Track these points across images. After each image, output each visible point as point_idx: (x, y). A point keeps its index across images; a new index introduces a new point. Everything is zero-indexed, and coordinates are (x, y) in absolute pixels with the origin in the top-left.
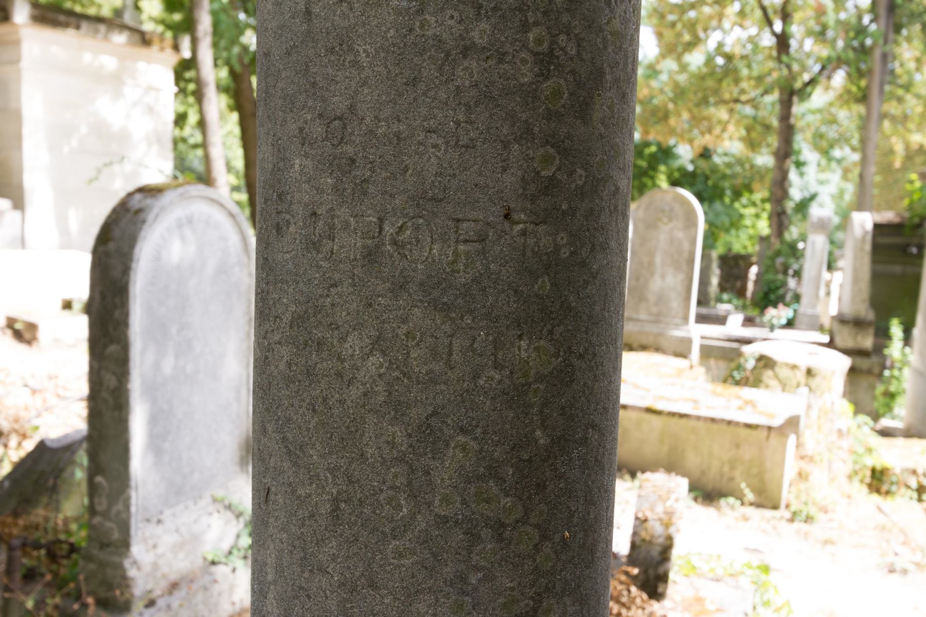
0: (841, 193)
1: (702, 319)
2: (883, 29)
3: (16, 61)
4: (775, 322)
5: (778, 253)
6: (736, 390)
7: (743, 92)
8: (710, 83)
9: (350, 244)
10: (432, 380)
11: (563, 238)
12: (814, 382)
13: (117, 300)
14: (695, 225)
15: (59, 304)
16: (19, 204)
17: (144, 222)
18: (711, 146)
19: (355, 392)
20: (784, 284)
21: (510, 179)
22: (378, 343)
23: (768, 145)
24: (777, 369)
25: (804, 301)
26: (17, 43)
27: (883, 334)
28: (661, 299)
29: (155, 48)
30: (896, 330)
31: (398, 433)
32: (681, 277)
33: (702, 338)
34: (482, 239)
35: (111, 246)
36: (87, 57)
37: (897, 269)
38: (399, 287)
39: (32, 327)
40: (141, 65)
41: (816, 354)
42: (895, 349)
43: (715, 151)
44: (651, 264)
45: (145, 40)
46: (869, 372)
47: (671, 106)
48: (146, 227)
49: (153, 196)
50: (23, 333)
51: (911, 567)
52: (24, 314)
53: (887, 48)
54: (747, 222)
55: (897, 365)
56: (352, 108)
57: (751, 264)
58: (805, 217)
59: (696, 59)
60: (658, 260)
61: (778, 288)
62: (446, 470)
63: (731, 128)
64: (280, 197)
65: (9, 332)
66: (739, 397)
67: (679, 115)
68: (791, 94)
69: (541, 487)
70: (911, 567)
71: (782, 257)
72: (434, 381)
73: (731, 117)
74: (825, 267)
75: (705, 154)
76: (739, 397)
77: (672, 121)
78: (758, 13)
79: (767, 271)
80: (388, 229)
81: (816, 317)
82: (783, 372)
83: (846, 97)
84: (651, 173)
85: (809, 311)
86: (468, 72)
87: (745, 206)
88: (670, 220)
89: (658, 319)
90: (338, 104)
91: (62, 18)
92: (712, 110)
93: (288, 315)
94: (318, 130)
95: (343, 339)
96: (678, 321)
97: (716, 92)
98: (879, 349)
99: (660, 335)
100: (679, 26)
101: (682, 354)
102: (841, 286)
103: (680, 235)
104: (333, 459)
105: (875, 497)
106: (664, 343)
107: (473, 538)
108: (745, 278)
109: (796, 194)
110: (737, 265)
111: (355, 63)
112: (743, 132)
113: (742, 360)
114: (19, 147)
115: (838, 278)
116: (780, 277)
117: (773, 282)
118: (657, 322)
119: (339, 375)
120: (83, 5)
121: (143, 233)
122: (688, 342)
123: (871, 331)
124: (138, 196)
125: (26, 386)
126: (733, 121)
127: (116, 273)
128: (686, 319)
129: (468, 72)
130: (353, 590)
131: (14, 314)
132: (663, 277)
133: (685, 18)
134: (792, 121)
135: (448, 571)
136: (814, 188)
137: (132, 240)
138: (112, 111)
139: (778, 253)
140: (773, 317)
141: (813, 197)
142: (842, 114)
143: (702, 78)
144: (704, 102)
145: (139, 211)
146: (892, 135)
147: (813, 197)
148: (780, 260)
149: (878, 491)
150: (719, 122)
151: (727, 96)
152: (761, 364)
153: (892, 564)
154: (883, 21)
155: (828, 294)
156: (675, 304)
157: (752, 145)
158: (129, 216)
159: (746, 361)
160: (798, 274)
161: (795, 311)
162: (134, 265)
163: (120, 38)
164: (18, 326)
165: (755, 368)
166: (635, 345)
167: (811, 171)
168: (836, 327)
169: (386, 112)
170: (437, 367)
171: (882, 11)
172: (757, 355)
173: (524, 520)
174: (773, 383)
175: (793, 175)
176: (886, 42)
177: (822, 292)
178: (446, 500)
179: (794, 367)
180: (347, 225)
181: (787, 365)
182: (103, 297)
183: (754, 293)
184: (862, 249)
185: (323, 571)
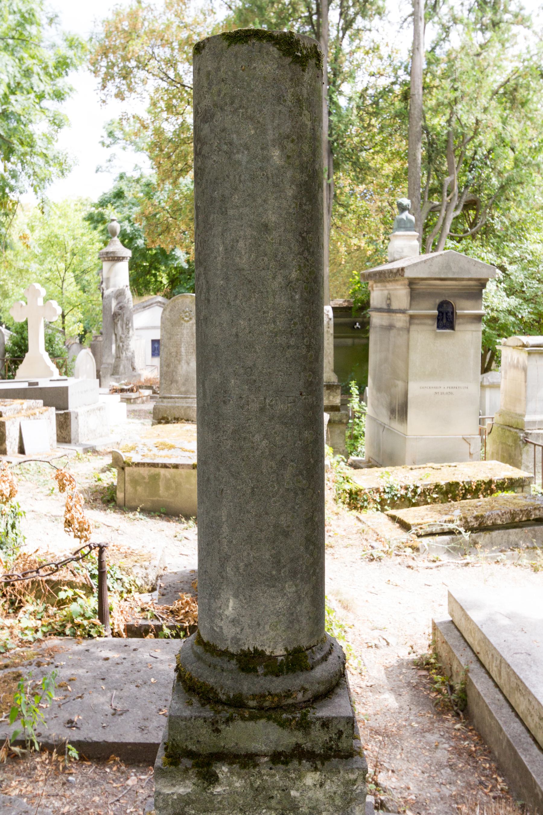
9: (255, 406)
10: (283, 446)
11: (314, 399)
19: (258, 453)
21: (301, 383)
22: (266, 436)
27: (346, 392)
30: (355, 390)
31: (273, 464)
34: (294, 402)
37: (349, 341)
38: (271, 418)
42: (355, 403)
46: (340, 422)
51: (382, 554)
55: (357, 415)
56: (254, 365)
60: (183, 350)
62: (288, 474)
64: (225, 392)
69: (313, 476)
70: (382, 554)
72: (283, 447)
80: (267, 401)
86: (289, 353)
90: (249, 363)
93: (231, 430)
94: (242, 371)
95: (253, 436)
98: (345, 403)
104: (251, 475)
105: (354, 512)
107: (296, 494)
111: (255, 352)
119: (253, 448)
123: (339, 391)
129: (289, 353)
130: (260, 516)
135: (289, 506)
149: (356, 508)
153: (372, 555)
169: (266, 366)
170: (284, 442)
173: (308, 488)
178: (288, 483)
180: (253, 401)
185: (248, 512)
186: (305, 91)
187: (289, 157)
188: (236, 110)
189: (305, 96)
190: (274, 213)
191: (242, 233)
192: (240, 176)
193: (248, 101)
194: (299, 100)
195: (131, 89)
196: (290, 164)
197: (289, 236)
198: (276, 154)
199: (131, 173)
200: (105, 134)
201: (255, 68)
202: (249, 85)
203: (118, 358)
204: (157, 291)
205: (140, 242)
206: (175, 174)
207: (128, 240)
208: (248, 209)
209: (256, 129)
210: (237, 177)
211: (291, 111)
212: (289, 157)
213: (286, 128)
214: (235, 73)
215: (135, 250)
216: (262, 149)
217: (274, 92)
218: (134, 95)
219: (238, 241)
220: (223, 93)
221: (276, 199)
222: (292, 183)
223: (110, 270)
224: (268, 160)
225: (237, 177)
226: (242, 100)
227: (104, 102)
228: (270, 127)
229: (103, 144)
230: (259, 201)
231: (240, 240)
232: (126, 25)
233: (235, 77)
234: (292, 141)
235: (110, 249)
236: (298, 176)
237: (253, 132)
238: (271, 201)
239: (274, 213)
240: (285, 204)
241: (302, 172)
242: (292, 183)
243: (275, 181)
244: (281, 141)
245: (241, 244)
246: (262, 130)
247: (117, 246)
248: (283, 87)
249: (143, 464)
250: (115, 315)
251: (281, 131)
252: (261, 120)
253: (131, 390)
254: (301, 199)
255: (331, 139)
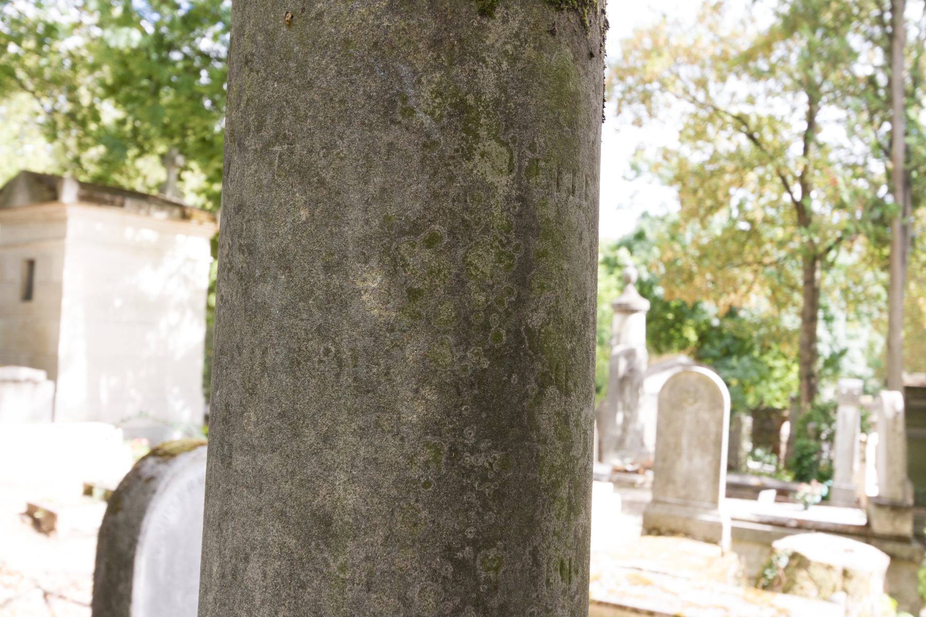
0: (871, 346)
1: (735, 490)
2: (901, 203)
3: (62, 237)
4: (808, 499)
5: (809, 419)
6: (767, 596)
7: (766, 254)
8: (732, 247)
12: (851, 585)
13: (122, 573)
14: (720, 406)
15: (81, 490)
16: (52, 375)
17: (154, 492)
18: (736, 304)
20: (820, 451)
23: (794, 305)
24: (811, 569)
25: (839, 474)
26: (63, 220)
28: (689, 481)
29: (194, 222)
32: (708, 459)
33: (733, 519)
35: (121, 516)
36: (129, 233)
39: (51, 516)
40: (180, 238)
41: (851, 551)
43: (741, 309)
44: (677, 445)
45: (185, 216)
47: (695, 269)
48: (156, 497)
49: (166, 462)
50: (41, 522)
52: (45, 504)
53: (906, 221)
54: (777, 374)
57: (783, 420)
58: (837, 369)
59: (719, 221)
60: (684, 441)
61: (810, 455)
63: (756, 287)
65: (28, 520)
66: (772, 606)
67: (703, 275)
68: (814, 259)
71: (816, 421)
73: (756, 277)
74: (858, 429)
75: (731, 313)
76: (772, 606)
77: (698, 281)
78: (778, 180)
79: (798, 436)
81: (850, 492)
82: (818, 573)
83: (869, 259)
84: (678, 325)
85: (844, 486)
87: (775, 358)
88: (696, 401)
89: (686, 502)
91: (107, 197)
92: (736, 271)
96: (707, 504)
97: (740, 253)
99: (688, 519)
100: (701, 193)
101: (712, 539)
102: (877, 448)
103: (706, 416)
106: (693, 528)
108: (777, 431)
109: (824, 349)
110: (769, 419)
112: (769, 292)
113: (774, 558)
114: (58, 319)
115: (874, 439)
116: (812, 443)
117: (806, 447)
118: (685, 505)
120: (129, 178)
121: (152, 504)
122: (718, 527)
124: (151, 461)
125: (38, 587)
126: (758, 281)
127: (123, 546)
128: (715, 502)
131: (35, 501)
132: (690, 458)
133: (706, 185)
134: (816, 284)
136: (843, 343)
137: (141, 512)
138: (150, 281)
139: (809, 419)
140: (806, 494)
141: (843, 353)
142: (868, 276)
143: (723, 241)
144: (728, 261)
145: (151, 479)
146: (920, 296)
147: (843, 353)
148: (811, 426)
150: (744, 282)
151: (750, 258)
152: (795, 562)
154: (900, 195)
155: (864, 460)
156: (704, 487)
157: (779, 304)
158: (140, 484)
159: (778, 558)
160: (831, 438)
161: (829, 488)
162: (141, 538)
163: (160, 215)
164: (38, 515)
165: (787, 567)
166: (663, 529)
167: (840, 326)
168: (873, 510)
171: (899, 186)
172: (789, 553)
174: (808, 585)
175: (821, 330)
176: (904, 215)
177: (857, 465)
179: (829, 567)
181: (821, 564)
182: (109, 569)
183: (787, 455)
184: (894, 430)
186: (488, 80)
187: (414, 294)
188: (267, 147)
189: (490, 92)
190: (352, 480)
191: (258, 535)
192: (265, 352)
193: (299, 119)
194: (461, 108)
195: (651, 115)
196: (416, 316)
197: (405, 559)
198: (370, 284)
199: (655, 212)
200: (628, 168)
201: (320, 15)
202: (302, 67)
203: (624, 429)
204: (683, 348)
205: (659, 291)
206: (702, 211)
207: (645, 289)
208: (277, 459)
209: (313, 203)
210: (258, 352)
211: (429, 145)
212: (414, 294)
213: (410, 201)
214: (270, 36)
215: (655, 301)
216: (327, 268)
217: (373, 86)
218: (654, 121)
219: (247, 559)
220: (245, 98)
221: (362, 433)
222: (423, 381)
223: (622, 324)
224: (344, 305)
225: (258, 352)
226: (281, 116)
227: (618, 130)
228: (355, 197)
229: (624, 178)
230: (310, 436)
231: (253, 558)
232: (647, 43)
233: (270, 48)
234: (431, 242)
235: (624, 299)
236: (447, 356)
237: (304, 214)
238: (347, 439)
239: (352, 480)
240: (392, 450)
241: (464, 342)
242: (423, 381)
243: (362, 372)
244: (387, 244)
245: (253, 571)
246: (330, 208)
247: (632, 296)
248: (404, 70)
249: (607, 604)
250: (624, 380)
251: (392, 211)
252: (328, 176)
253: (636, 472)
254: (459, 432)
255: (909, 167)
